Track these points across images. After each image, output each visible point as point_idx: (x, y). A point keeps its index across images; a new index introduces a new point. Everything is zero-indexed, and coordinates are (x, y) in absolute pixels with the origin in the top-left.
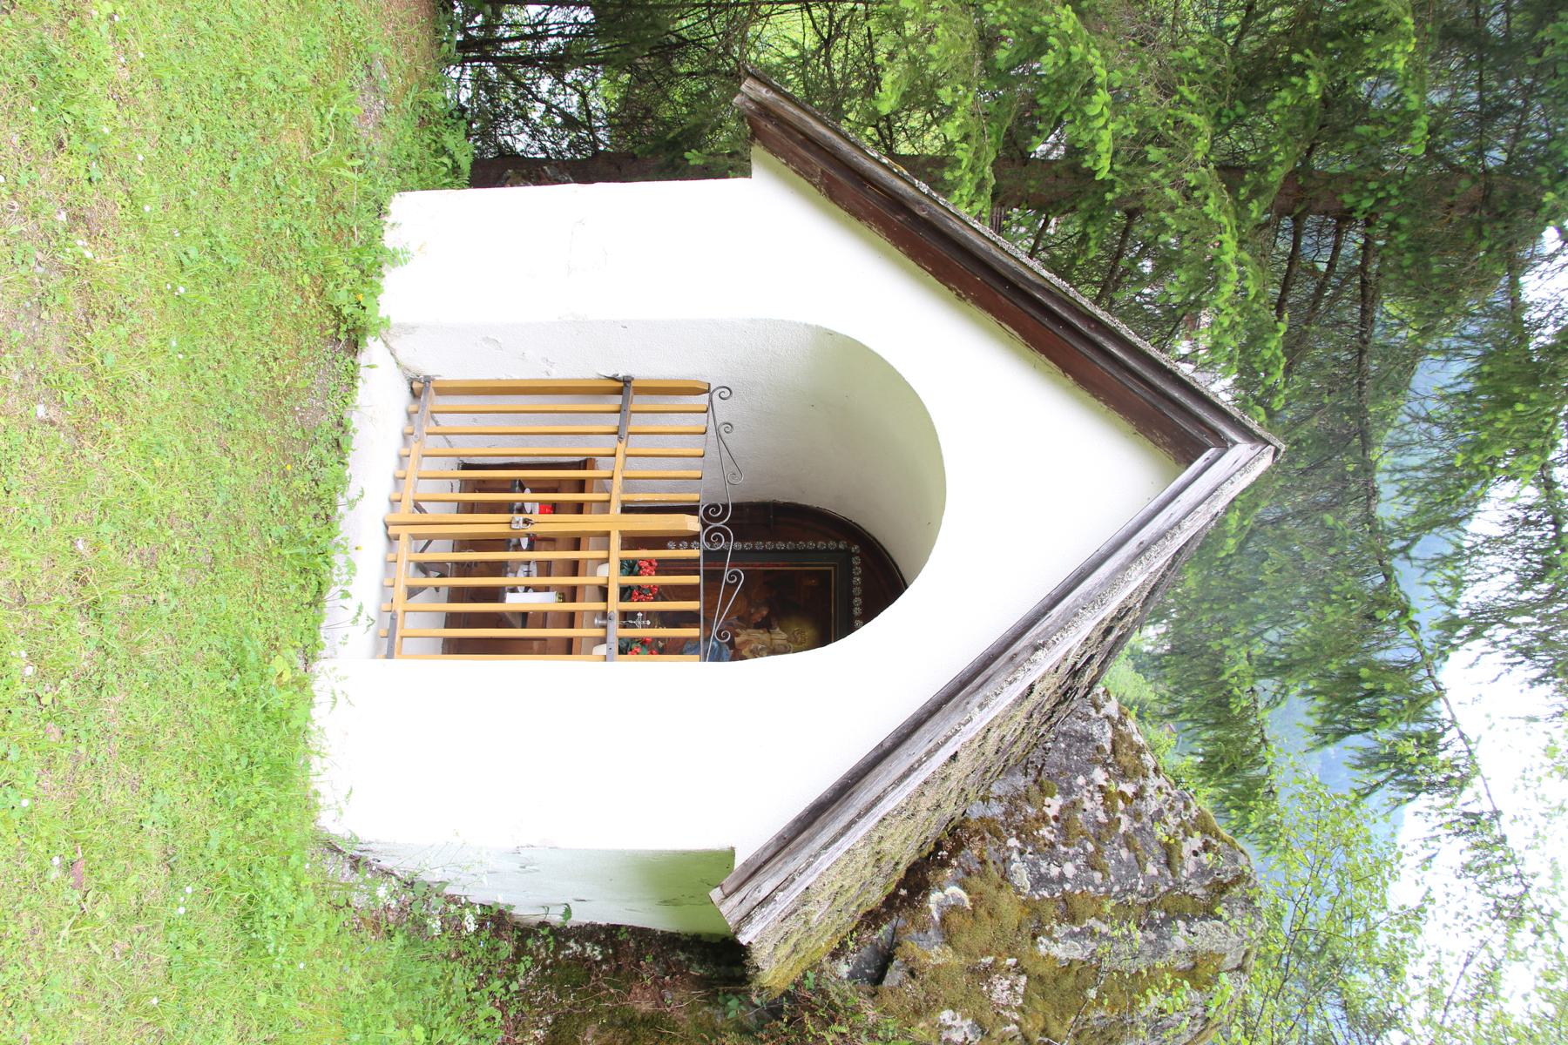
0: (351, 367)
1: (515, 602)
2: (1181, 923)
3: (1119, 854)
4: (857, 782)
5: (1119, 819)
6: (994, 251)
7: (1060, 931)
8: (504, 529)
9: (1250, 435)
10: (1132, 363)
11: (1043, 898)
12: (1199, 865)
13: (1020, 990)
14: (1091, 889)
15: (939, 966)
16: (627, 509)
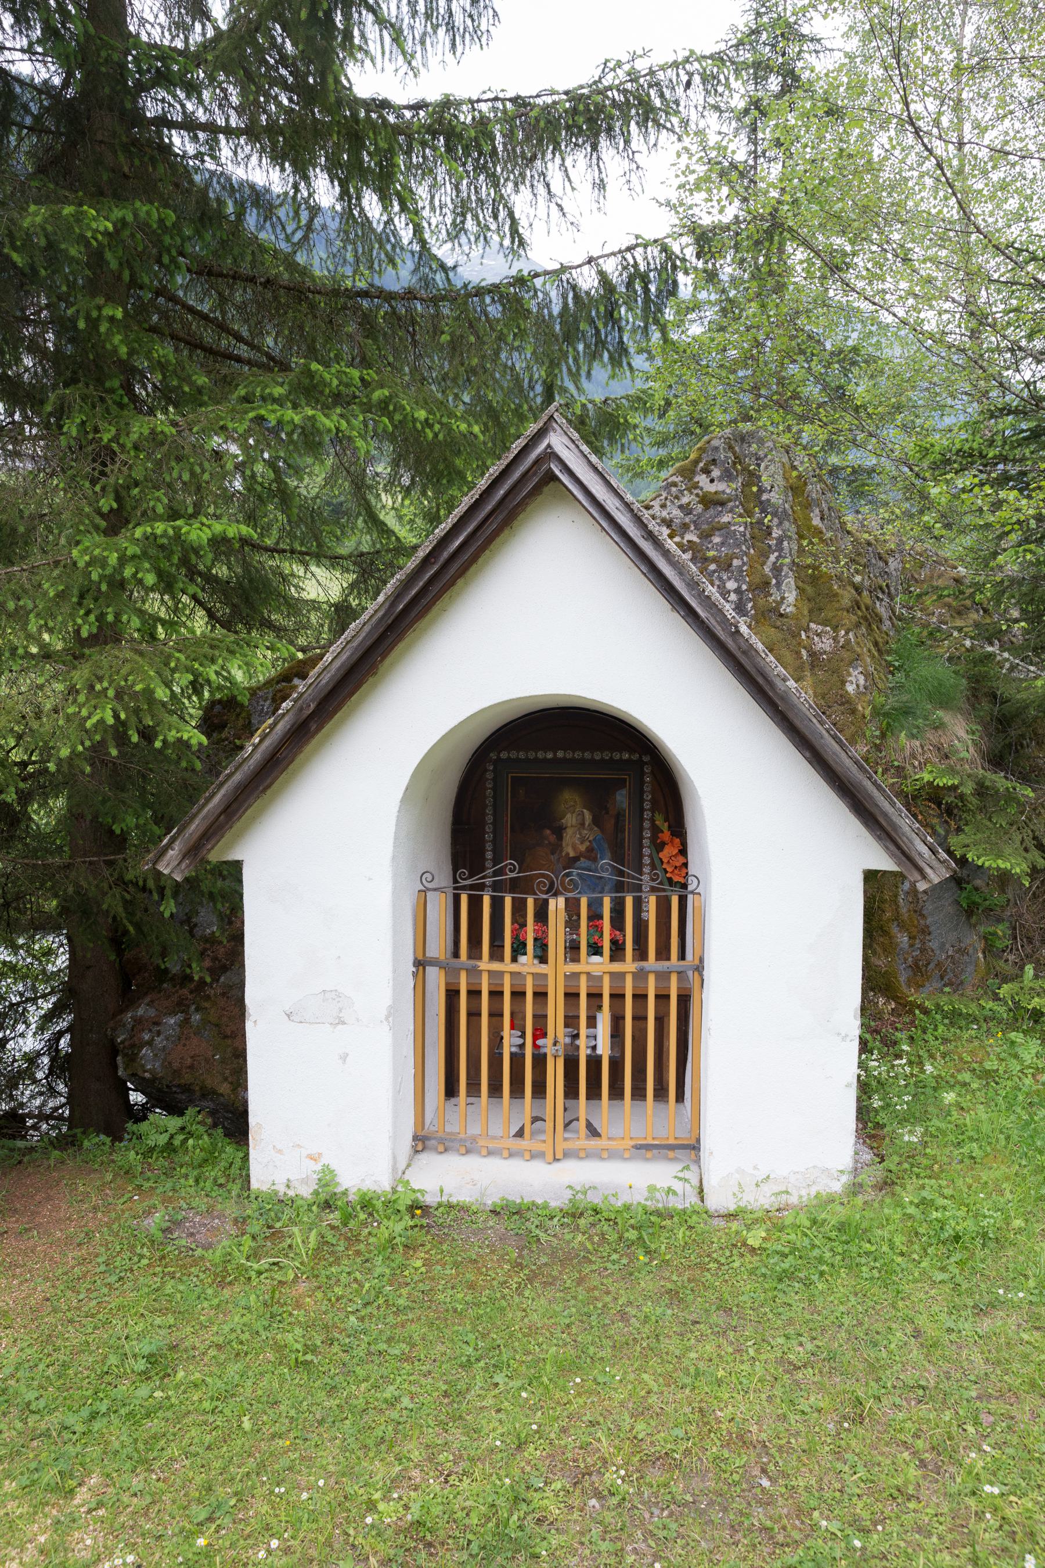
0: (441, 1210)
1: (604, 1049)
2: (765, 497)
4: (839, 778)
6: (355, 644)
7: (776, 596)
9: (541, 433)
10: (470, 529)
12: (721, 479)
13: (820, 628)
15: (815, 693)
16: (543, 959)
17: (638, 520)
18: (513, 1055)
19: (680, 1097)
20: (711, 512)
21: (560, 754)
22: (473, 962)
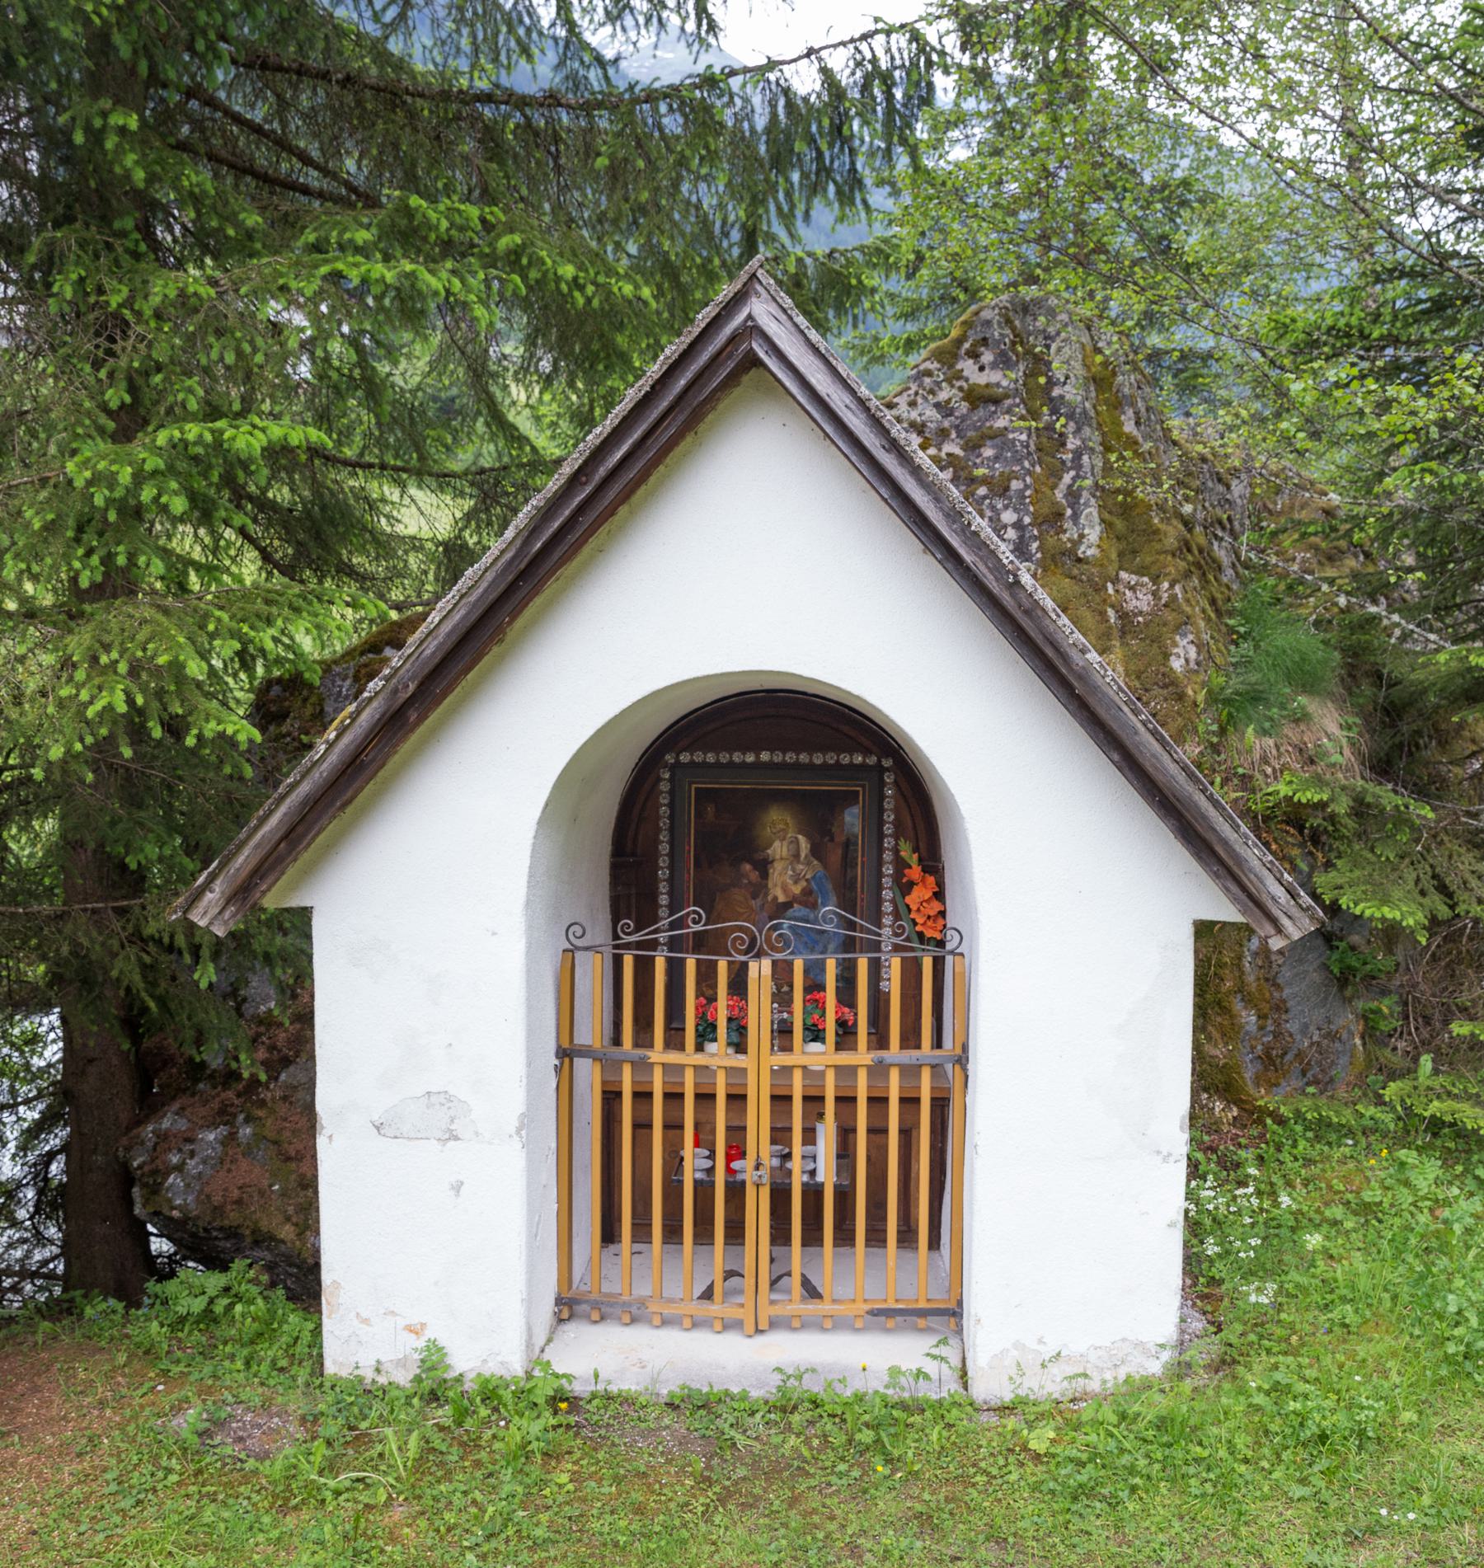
1: (827, 1174)
2: (1056, 392)
3: (988, 459)
4: (1160, 791)
5: (948, 455)
6: (472, 598)
7: (1072, 533)
8: (765, 1193)
9: (739, 298)
10: (637, 434)
11: (1039, 549)
12: (994, 366)
13: (1133, 579)
14: (1028, 493)
17: (876, 423)
18: (696, 1182)
19: (934, 1243)
20: (981, 412)
21: (765, 756)
22: (640, 1052)
